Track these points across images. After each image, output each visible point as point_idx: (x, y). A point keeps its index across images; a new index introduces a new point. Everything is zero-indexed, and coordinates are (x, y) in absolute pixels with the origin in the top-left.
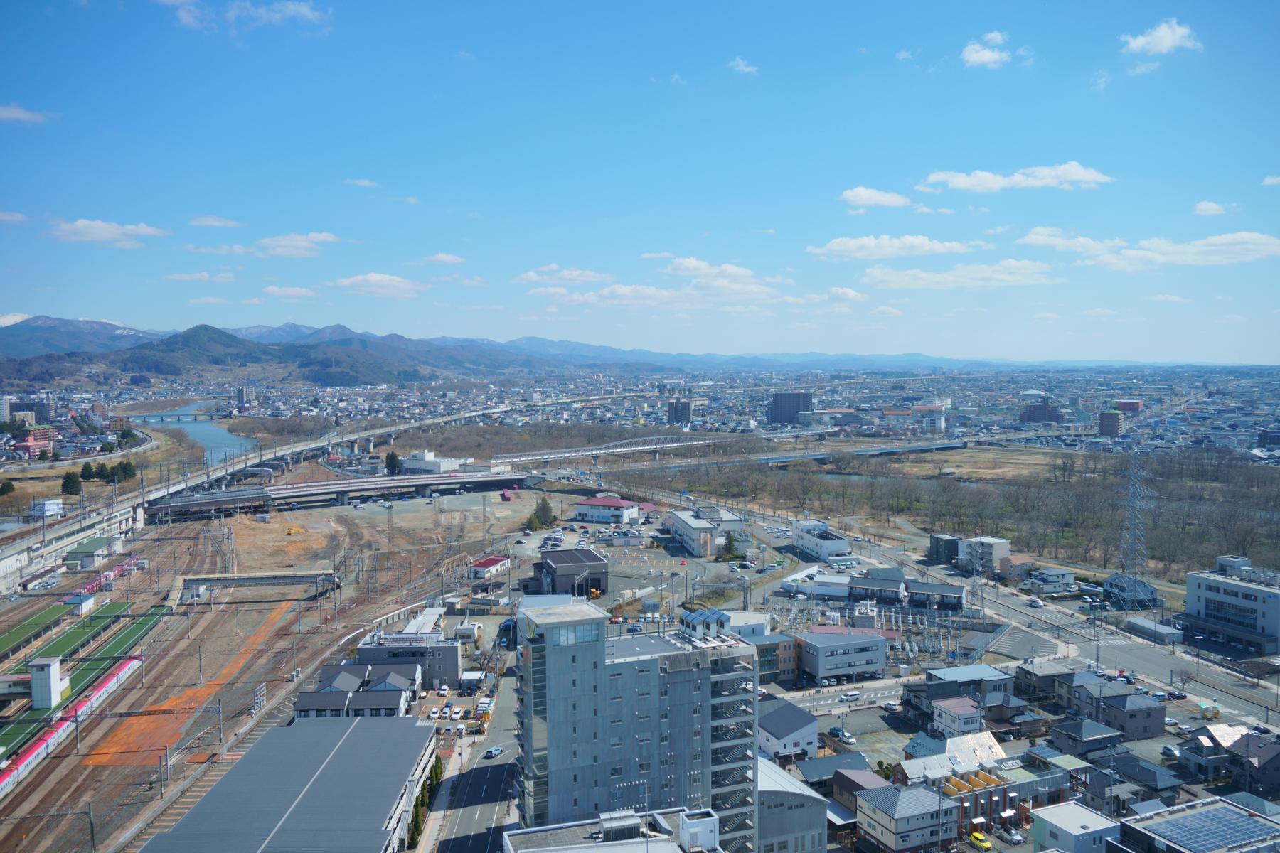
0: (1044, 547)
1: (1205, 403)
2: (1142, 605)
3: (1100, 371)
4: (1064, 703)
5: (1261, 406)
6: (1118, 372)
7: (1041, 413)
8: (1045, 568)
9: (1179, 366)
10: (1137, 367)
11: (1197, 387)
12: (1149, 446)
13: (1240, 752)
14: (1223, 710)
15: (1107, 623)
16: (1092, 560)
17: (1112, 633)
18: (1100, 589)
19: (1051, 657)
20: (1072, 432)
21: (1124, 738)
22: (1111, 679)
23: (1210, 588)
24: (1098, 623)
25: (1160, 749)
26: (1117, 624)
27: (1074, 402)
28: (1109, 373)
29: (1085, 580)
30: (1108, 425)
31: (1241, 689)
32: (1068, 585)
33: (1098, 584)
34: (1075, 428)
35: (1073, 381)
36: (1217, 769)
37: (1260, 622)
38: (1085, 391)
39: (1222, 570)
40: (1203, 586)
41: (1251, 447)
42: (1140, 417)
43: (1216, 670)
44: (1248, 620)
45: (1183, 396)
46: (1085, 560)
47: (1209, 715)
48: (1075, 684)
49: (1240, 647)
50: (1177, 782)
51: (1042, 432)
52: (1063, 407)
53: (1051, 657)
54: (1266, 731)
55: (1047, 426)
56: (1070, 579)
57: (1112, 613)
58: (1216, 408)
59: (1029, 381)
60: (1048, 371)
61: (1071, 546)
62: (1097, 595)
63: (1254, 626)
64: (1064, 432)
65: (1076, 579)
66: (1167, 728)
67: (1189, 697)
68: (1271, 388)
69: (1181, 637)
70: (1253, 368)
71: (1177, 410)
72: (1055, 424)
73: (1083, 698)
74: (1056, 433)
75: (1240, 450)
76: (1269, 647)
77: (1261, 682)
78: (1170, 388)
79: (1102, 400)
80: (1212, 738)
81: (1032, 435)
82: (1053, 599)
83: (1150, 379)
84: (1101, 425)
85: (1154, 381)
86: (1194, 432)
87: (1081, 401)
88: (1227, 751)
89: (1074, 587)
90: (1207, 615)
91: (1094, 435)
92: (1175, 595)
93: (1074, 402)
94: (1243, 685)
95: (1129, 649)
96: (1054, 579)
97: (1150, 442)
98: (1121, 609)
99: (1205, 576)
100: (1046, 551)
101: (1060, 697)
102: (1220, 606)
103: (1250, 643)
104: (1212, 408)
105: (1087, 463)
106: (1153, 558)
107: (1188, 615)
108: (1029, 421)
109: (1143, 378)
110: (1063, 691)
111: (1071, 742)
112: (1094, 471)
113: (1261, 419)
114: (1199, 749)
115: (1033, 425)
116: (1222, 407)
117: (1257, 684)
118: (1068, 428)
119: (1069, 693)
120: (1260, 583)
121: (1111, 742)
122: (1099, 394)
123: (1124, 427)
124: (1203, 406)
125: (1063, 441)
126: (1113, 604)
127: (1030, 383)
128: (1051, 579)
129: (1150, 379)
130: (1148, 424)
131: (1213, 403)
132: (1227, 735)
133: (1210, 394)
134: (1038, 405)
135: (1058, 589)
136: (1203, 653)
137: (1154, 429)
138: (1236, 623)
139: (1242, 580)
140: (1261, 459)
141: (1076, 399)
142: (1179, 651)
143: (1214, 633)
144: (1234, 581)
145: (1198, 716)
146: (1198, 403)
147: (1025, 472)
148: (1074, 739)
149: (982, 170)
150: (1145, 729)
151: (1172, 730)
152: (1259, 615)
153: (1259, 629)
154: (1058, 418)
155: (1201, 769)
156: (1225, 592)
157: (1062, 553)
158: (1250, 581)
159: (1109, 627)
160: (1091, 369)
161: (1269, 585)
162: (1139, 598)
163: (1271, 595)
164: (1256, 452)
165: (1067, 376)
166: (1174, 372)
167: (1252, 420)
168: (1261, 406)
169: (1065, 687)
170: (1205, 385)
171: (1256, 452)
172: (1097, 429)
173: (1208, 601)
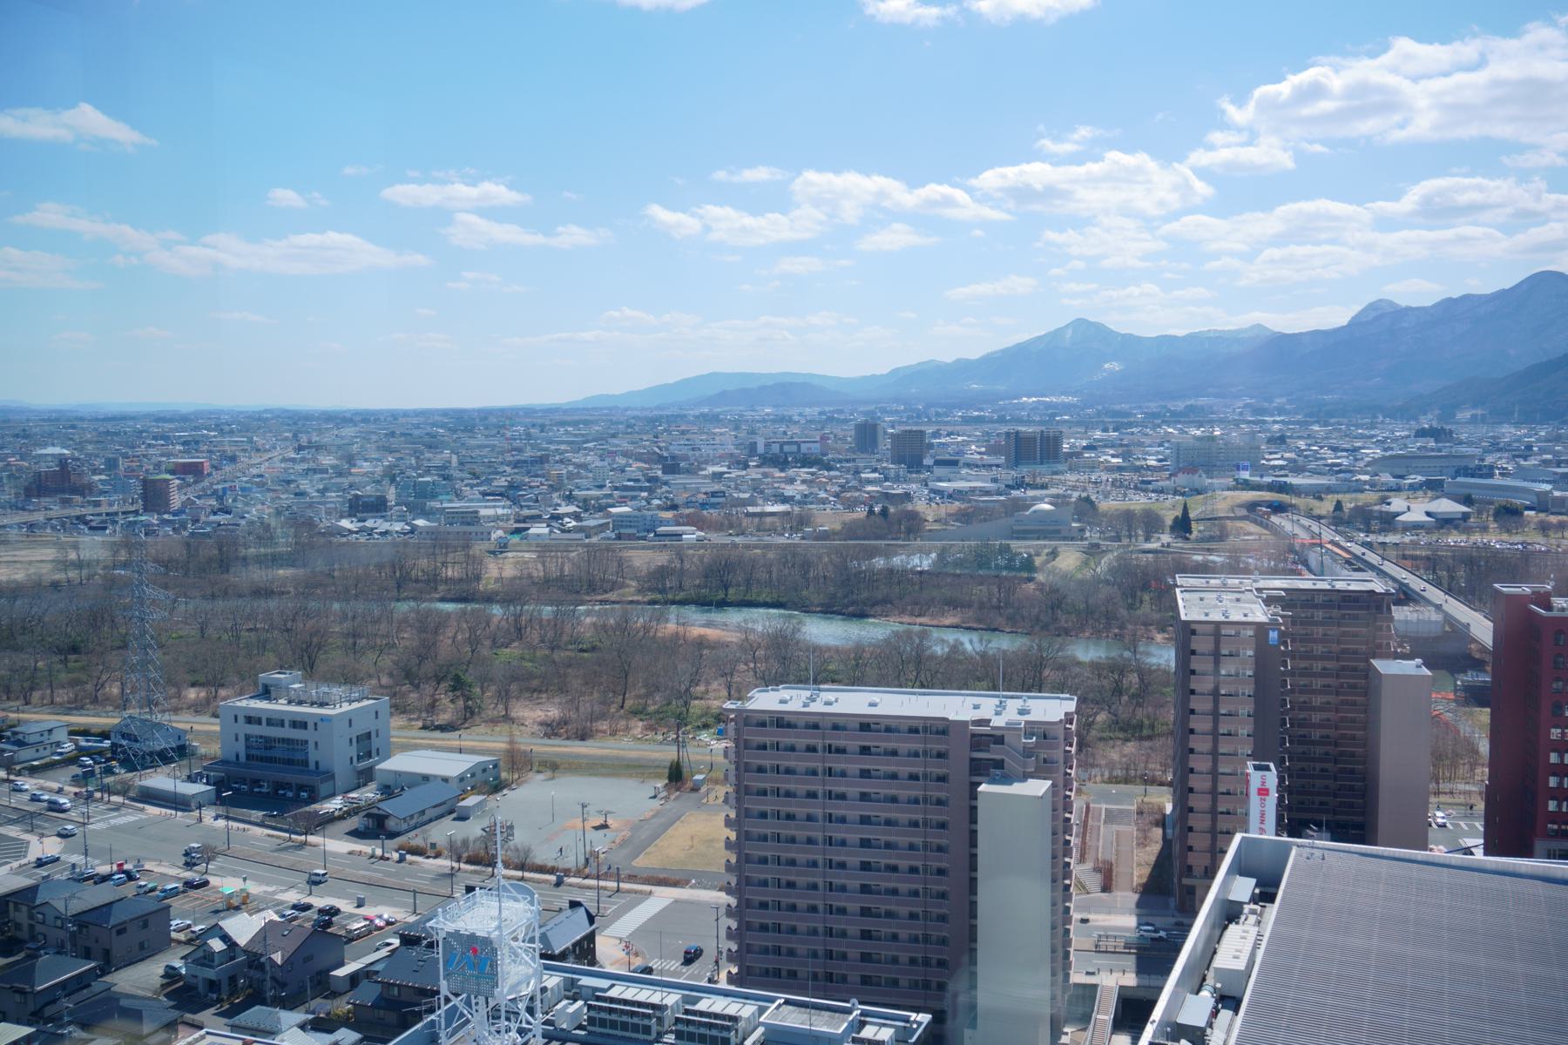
0: (32, 689)
1: (293, 460)
2: (164, 758)
3: (159, 419)
4: (24, 934)
5: (360, 463)
6: (183, 419)
7: (60, 482)
8: (27, 722)
9: (266, 411)
10: (210, 412)
11: (286, 439)
12: (208, 523)
13: (258, 949)
14: (254, 888)
15: (110, 793)
16: (108, 699)
17: (118, 808)
18: (107, 743)
19: (15, 864)
20: (104, 509)
21: (104, 971)
22: (105, 878)
23: (249, 720)
24: (98, 795)
25: (161, 971)
26: (123, 793)
27: (111, 464)
28: (171, 420)
29: (85, 733)
30: (153, 496)
31: (283, 855)
32: (58, 744)
33: (104, 735)
34: (111, 503)
35: (117, 434)
36: (233, 980)
37: (313, 756)
38: (133, 447)
39: (266, 693)
40: (241, 719)
41: (342, 517)
42: (206, 483)
43: (256, 834)
44: (299, 756)
45: (266, 451)
46: (95, 701)
47: (235, 902)
48: (38, 902)
49: (290, 794)
50: (175, 1014)
51: (57, 511)
52: (95, 471)
53: (15, 864)
54: (307, 907)
55: (66, 503)
56: (61, 735)
57: (122, 774)
58: (305, 466)
59: (51, 434)
60: (82, 419)
61: (74, 683)
62: (101, 752)
63: (306, 763)
64: (91, 510)
65: (71, 733)
66: (174, 935)
67: (214, 881)
68: (374, 438)
69: (213, 796)
70: (357, 413)
71: (254, 471)
72: (78, 498)
73: (50, 920)
74: (77, 512)
75: (324, 524)
76: (324, 788)
77: (311, 839)
78: (251, 441)
79: (154, 460)
80: (225, 938)
81: (39, 517)
82: (33, 771)
83: (227, 428)
84: (145, 497)
85: (231, 432)
86: (273, 500)
87: (122, 464)
88: (245, 951)
89: (68, 747)
90: (248, 757)
91: (136, 513)
92: (208, 733)
93: (111, 464)
94: (286, 849)
95: (137, 828)
96: (37, 738)
97: (212, 518)
98: (133, 769)
99: (244, 703)
100: (36, 695)
101: (18, 926)
102: (269, 742)
103: (302, 788)
104: (300, 467)
105: (115, 553)
106: (193, 685)
107: (224, 762)
108: (39, 496)
109: (218, 427)
110: (22, 916)
111: (18, 997)
112: (125, 565)
113: (357, 479)
114: (207, 958)
115: (45, 501)
116: (312, 465)
117: (305, 843)
118: (97, 504)
119: (31, 917)
120: (312, 704)
121: (81, 982)
122: (151, 451)
123: (176, 500)
124: (290, 465)
125: (86, 523)
126: (123, 763)
127: (49, 438)
128: (31, 739)
129: (227, 428)
130: (215, 492)
131: (303, 460)
132: (244, 929)
133: (300, 448)
134: (445, 413)
135: (42, 753)
136: (234, 811)
137: (220, 499)
138: (262, 759)
139: (290, 702)
140: (351, 532)
141: (115, 460)
142: (208, 814)
143: (256, 782)
144: (280, 706)
145: (220, 906)
146: (284, 460)
147: (20, 576)
148: (22, 992)
149: (97, 107)
150: (142, 946)
151: (182, 937)
152: (311, 745)
153: (312, 766)
154: (84, 490)
155: (213, 985)
156: (270, 722)
157: (62, 696)
158: (300, 703)
159: (114, 798)
160: (147, 416)
161: (322, 705)
162: (158, 748)
163: (323, 718)
164: (345, 523)
165: (110, 427)
166: (259, 419)
167: (345, 481)
168: (360, 463)
169: (24, 909)
170: (295, 436)
171: (345, 523)
172: (139, 505)
173: (247, 737)
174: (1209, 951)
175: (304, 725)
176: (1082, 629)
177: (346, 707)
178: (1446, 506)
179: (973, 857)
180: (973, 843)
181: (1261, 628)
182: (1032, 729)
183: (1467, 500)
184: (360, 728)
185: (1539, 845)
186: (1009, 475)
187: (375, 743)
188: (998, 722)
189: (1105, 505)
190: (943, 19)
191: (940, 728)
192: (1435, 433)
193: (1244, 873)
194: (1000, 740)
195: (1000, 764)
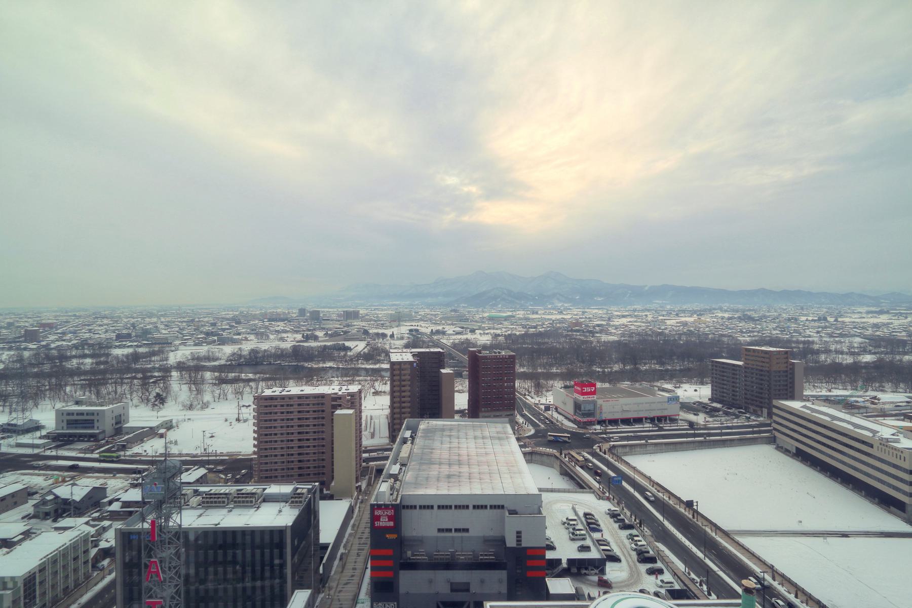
23: (69, 414)
152: (96, 422)
174: (399, 452)
175: (93, 414)
176: (264, 356)
177: (111, 406)
178: (458, 329)
179: (333, 469)
180: (333, 465)
181: (411, 363)
182: (349, 394)
183: (462, 328)
184: (116, 413)
185: (481, 414)
186: (345, 323)
187: (123, 418)
188: (340, 393)
189: (371, 331)
190: (324, 363)
191: (322, 396)
192: (455, 311)
193: (408, 429)
194: (340, 398)
195: (340, 406)
